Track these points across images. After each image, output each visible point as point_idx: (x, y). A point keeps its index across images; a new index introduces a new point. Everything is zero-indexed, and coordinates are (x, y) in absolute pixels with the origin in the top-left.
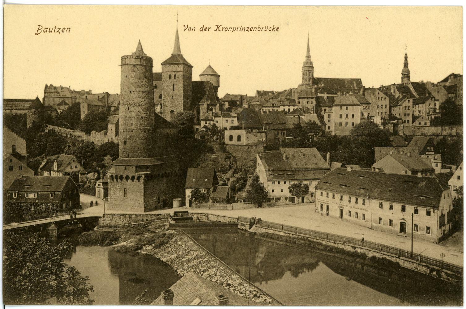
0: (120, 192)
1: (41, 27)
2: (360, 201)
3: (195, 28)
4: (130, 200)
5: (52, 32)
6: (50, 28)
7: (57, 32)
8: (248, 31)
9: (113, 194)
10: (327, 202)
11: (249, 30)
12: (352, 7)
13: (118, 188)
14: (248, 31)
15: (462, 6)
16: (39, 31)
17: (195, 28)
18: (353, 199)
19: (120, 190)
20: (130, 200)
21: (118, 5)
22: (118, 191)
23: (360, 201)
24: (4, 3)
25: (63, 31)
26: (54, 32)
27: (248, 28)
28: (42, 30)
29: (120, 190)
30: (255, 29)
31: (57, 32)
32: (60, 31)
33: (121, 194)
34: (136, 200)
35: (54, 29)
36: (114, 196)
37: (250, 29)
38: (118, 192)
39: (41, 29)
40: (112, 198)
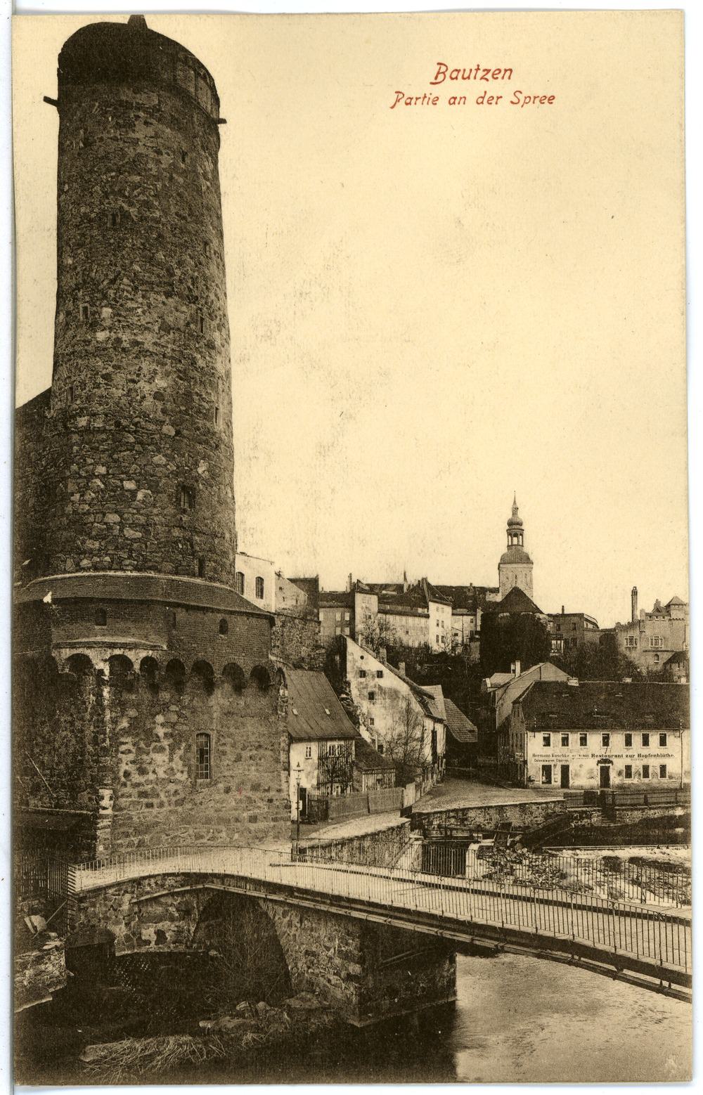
0: (171, 754)
1: (443, 69)
2: (654, 739)
3: (511, 70)
4: (227, 790)
5: (469, 78)
6: (464, 70)
7: (482, 78)
8: (487, 80)
9: (131, 768)
10: (564, 758)
11: (489, 76)
12: (409, 15)
13: (161, 731)
14: (487, 80)
15: (681, 13)
16: (441, 77)
17: (511, 70)
18: (637, 739)
19: (173, 749)
20: (227, 790)
21: (411, 13)
22: (162, 750)
23: (654, 739)
24: (15, 12)
25: (495, 76)
26: (475, 78)
27: (488, 71)
28: (448, 74)
29: (173, 749)
30: (466, 76)
31: (482, 78)
32: (489, 76)
33: (177, 764)
34: (256, 787)
35: (474, 72)
36: (141, 779)
37: (493, 74)
38: (160, 758)
39: (444, 73)
40: (128, 790)
